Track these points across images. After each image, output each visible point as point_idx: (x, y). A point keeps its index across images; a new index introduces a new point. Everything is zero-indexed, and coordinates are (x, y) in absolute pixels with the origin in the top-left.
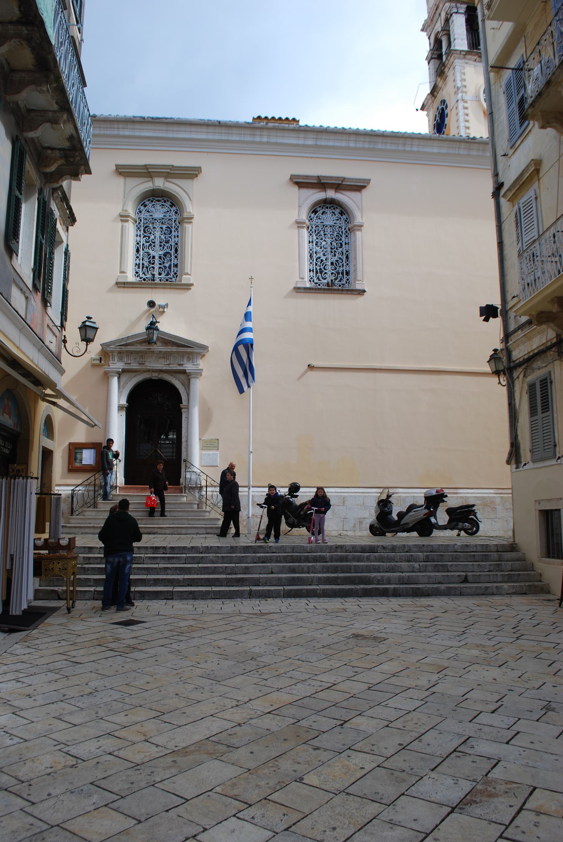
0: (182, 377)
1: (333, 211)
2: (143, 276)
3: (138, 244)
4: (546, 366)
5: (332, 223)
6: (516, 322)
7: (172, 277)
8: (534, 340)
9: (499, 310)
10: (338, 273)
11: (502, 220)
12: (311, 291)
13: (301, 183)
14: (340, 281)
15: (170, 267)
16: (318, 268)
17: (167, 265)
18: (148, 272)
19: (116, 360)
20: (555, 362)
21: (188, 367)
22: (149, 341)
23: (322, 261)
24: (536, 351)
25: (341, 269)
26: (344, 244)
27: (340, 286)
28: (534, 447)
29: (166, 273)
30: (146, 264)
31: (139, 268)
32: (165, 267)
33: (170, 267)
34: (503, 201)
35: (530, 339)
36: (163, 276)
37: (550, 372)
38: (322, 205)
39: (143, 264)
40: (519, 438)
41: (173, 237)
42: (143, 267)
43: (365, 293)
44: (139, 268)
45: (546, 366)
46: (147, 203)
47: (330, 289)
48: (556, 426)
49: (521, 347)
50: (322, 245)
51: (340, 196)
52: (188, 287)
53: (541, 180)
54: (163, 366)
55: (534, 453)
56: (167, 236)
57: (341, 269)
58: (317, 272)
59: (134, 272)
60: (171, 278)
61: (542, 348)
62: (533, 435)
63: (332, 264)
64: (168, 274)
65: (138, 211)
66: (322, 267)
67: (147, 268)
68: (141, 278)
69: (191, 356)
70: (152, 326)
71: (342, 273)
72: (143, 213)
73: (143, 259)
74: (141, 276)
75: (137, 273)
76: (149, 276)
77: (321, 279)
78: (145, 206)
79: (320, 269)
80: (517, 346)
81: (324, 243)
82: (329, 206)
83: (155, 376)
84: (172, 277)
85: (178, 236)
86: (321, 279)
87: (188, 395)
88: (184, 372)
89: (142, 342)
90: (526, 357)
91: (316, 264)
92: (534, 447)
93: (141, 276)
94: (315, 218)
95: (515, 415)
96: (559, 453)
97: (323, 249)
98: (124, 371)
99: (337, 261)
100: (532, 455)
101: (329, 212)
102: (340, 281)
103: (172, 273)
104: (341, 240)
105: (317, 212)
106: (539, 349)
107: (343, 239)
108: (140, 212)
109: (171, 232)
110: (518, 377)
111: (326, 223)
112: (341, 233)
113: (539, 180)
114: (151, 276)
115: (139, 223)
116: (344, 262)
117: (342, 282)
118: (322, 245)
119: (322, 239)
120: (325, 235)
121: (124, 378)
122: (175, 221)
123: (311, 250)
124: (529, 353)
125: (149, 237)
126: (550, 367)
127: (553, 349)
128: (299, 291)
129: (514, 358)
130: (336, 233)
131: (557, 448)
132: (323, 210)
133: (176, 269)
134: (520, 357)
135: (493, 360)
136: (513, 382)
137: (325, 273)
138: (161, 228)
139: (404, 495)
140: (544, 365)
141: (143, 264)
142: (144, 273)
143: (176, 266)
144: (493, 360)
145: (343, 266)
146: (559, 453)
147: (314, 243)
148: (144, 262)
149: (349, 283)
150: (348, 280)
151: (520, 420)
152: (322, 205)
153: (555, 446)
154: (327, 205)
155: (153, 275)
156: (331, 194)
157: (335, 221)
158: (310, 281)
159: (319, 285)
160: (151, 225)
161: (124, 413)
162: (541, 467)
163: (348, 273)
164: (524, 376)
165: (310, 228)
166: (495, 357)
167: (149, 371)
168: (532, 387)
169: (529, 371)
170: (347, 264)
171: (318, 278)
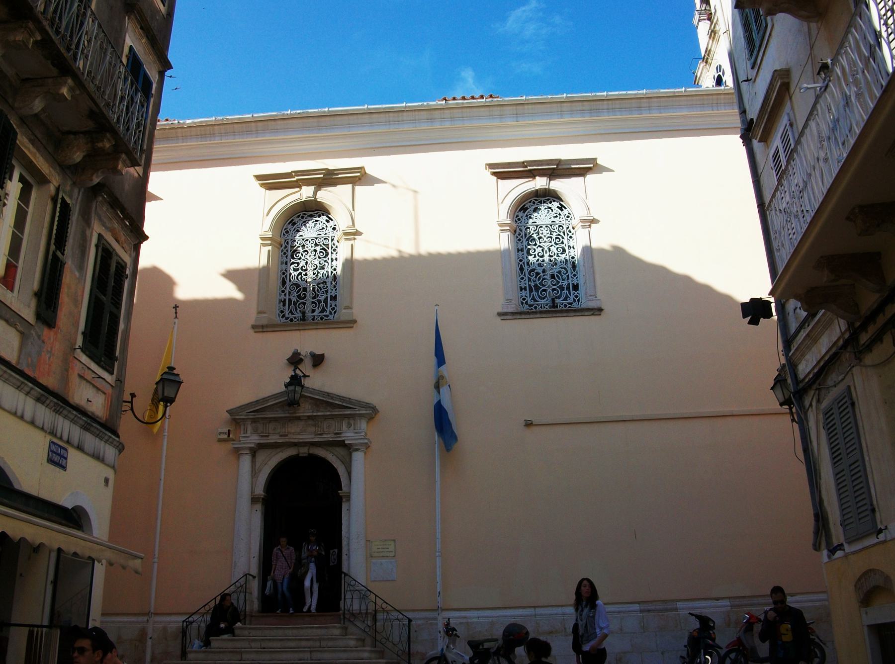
0: (341, 451)
1: (549, 205)
2: (291, 316)
3: (284, 274)
4: (843, 380)
5: (549, 222)
6: (796, 318)
7: (328, 313)
8: (821, 340)
9: (773, 305)
10: (562, 288)
11: (760, 172)
12: (523, 316)
13: (503, 172)
14: (565, 299)
15: (326, 301)
16: (532, 284)
17: (322, 298)
18: (296, 310)
19: (249, 432)
20: (854, 369)
21: (349, 436)
22: (292, 403)
23: (537, 274)
24: (827, 358)
25: (566, 282)
26: (567, 248)
27: (565, 306)
28: (846, 517)
29: (320, 309)
30: (294, 299)
31: (284, 305)
32: (320, 301)
33: (326, 301)
34: (755, 143)
35: (815, 341)
36: (316, 313)
37: (849, 387)
38: (533, 200)
39: (290, 300)
40: (826, 503)
41: (329, 261)
42: (290, 304)
43: (602, 313)
44: (284, 305)
45: (843, 380)
46: (296, 220)
47: (554, 310)
48: (870, 477)
49: (807, 357)
50: (536, 253)
51: (557, 185)
52: (350, 323)
53: (793, 98)
54: (313, 436)
55: (848, 527)
56: (322, 261)
57: (566, 282)
58: (531, 291)
59: (278, 312)
60: (327, 316)
61: (834, 350)
62: (842, 496)
63: (553, 276)
64: (323, 310)
65: (284, 232)
66: (538, 283)
67: (295, 304)
68: (287, 319)
69: (352, 422)
70: (295, 380)
71: (568, 288)
72: (290, 233)
73: (290, 293)
74: (287, 316)
75: (282, 312)
76: (298, 315)
77: (538, 299)
78: (294, 224)
79: (536, 286)
80: (803, 355)
81: (540, 249)
82: (543, 199)
83: (304, 451)
84: (328, 313)
85: (336, 259)
86: (538, 299)
87: (349, 474)
88: (342, 444)
89: (281, 405)
90: (816, 370)
91: (530, 280)
92: (846, 517)
93: (287, 316)
94: (524, 217)
95: (815, 467)
96: (881, 522)
97: (538, 257)
98: (261, 446)
99: (560, 272)
100: (844, 531)
101: (542, 208)
102: (565, 299)
103: (329, 309)
104: (563, 243)
105: (527, 209)
106: (831, 353)
107: (565, 241)
108: (287, 232)
109: (327, 254)
110: (811, 405)
111: (539, 222)
112: (562, 234)
113: (791, 98)
114: (301, 315)
115: (286, 247)
116: (569, 273)
117: (569, 301)
118: (536, 253)
119: (535, 245)
120: (540, 238)
121: (261, 456)
122: (332, 240)
123: (521, 261)
124: (818, 362)
125: (298, 264)
126: (848, 381)
127: (849, 349)
128: (505, 317)
129: (801, 376)
130: (555, 234)
131: (878, 515)
132: (535, 206)
133: (333, 303)
134: (809, 373)
135: (778, 386)
136: (806, 414)
137: (545, 290)
138: (315, 251)
139: (810, 604)
140: (840, 378)
141: (290, 300)
142: (291, 312)
143: (334, 298)
144: (778, 386)
145: (568, 279)
146: (881, 522)
147: (525, 251)
148: (291, 297)
149: (579, 300)
150: (576, 296)
151: (822, 474)
152: (533, 200)
153: (873, 510)
154: (540, 199)
155: (304, 313)
156: (540, 183)
157: (553, 219)
158: (522, 303)
159: (536, 308)
160: (300, 249)
161: (259, 507)
162: (861, 550)
163: (576, 287)
164: (819, 401)
165: (518, 231)
166: (779, 382)
167: (295, 445)
168: (827, 413)
169: (823, 392)
170: (575, 275)
171: (534, 299)
